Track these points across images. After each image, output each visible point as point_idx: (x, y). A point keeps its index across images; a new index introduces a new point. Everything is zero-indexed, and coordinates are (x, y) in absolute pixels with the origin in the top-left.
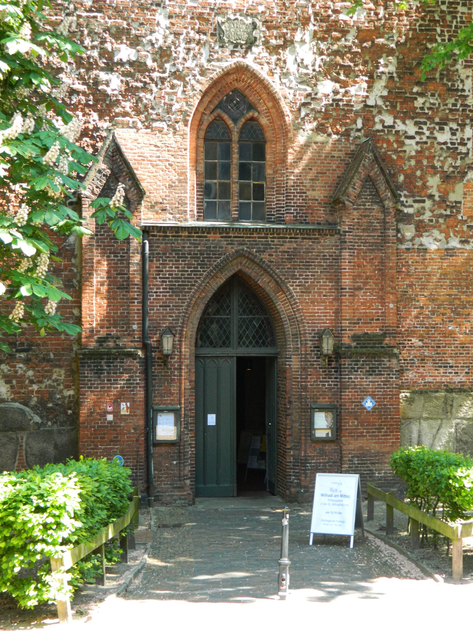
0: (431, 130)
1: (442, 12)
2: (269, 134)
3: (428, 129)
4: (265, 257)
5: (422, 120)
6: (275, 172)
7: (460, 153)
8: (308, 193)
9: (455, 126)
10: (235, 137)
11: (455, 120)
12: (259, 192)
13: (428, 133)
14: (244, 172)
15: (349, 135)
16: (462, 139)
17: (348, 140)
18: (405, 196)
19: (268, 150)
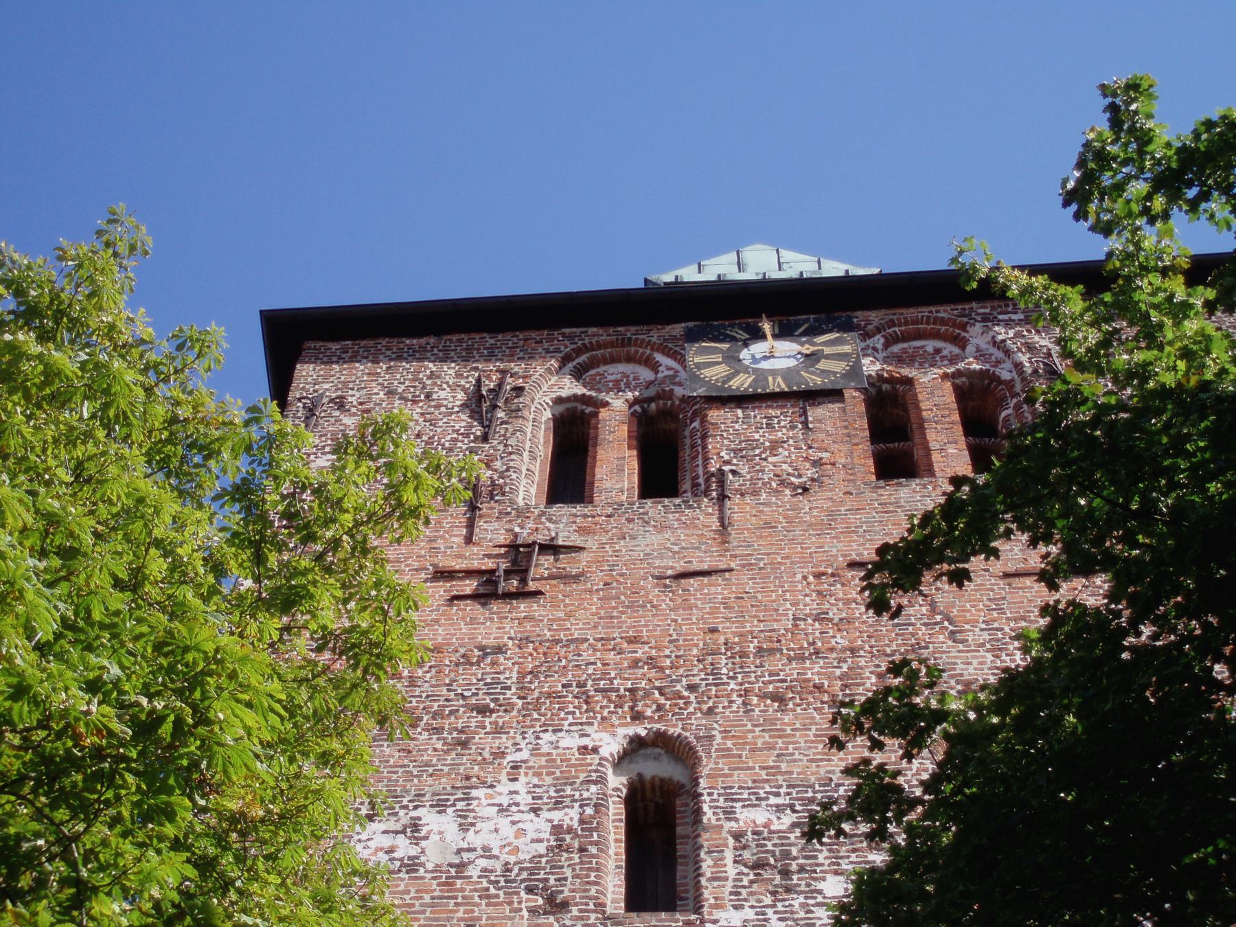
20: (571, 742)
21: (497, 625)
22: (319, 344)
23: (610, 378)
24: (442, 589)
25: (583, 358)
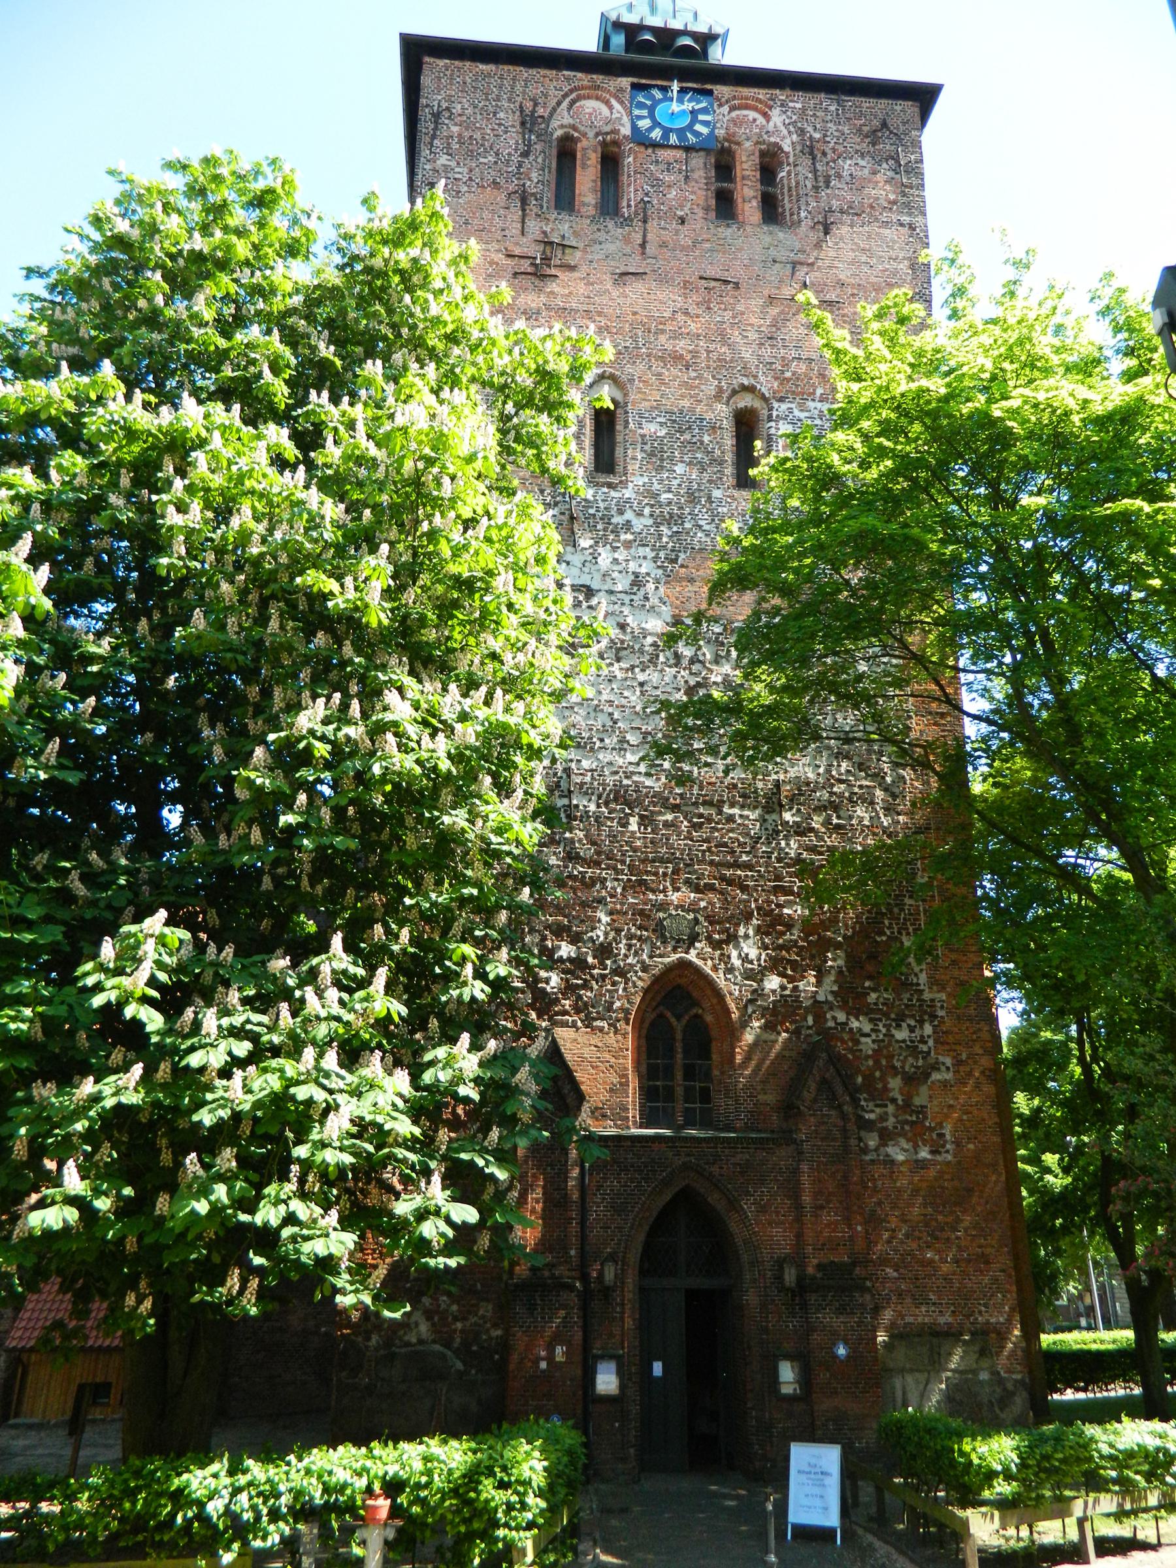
6: (722, 1073)
9: (913, 1023)
11: (913, 1016)
12: (705, 1095)
13: (884, 1030)
16: (922, 1036)
25: (573, 96)
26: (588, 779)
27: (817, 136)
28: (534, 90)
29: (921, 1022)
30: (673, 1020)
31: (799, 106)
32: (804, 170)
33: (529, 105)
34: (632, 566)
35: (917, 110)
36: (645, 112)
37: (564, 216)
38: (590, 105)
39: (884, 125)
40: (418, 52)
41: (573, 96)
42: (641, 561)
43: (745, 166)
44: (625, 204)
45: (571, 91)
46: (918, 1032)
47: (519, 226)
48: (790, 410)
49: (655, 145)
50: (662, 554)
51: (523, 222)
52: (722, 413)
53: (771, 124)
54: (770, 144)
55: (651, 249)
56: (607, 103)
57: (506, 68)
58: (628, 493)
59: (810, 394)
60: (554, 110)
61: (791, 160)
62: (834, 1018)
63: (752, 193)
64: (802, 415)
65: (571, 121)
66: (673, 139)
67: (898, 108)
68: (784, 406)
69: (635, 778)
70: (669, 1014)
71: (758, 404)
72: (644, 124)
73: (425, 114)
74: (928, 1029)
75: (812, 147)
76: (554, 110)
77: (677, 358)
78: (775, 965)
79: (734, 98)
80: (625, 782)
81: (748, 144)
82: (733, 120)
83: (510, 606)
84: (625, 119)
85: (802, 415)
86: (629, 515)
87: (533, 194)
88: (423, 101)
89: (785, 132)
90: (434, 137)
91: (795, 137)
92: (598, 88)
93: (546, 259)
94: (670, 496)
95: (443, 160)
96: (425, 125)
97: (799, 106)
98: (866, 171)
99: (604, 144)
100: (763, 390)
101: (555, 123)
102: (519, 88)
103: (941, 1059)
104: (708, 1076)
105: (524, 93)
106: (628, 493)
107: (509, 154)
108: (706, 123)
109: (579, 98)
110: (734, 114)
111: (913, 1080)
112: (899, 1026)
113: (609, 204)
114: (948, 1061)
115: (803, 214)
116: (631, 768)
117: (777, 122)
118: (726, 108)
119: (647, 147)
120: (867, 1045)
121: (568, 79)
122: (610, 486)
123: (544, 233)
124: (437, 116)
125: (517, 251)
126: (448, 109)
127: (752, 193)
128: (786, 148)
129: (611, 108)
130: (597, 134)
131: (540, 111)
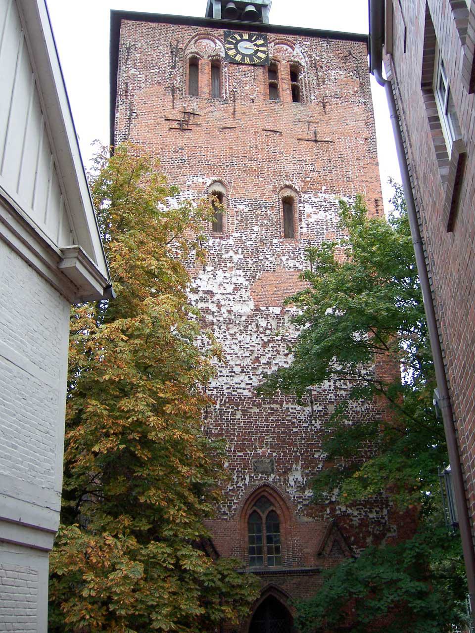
0: (366, 512)
1: (365, 451)
2: (282, 518)
3: (364, 511)
4: (284, 587)
5: (361, 507)
6: (286, 539)
7: (382, 523)
8: (304, 550)
9: (378, 509)
10: (264, 521)
11: (378, 506)
12: (278, 550)
13: (364, 514)
14: (270, 539)
15: (323, 517)
16: (382, 516)
17: (322, 519)
18: (356, 549)
19: (281, 527)
20: (201, 180)
21: (181, 140)
22: (126, 21)
23: (203, 44)
24: (167, 125)
25: (197, 38)
26: (215, 392)
27: (318, 58)
28: (176, 36)
29: (382, 509)
30: (261, 513)
31: (308, 43)
32: (312, 76)
33: (174, 43)
34: (234, 280)
35: (365, 46)
36: (232, 46)
37: (194, 99)
38: (205, 42)
39: (350, 53)
40: (118, 19)
41: (197, 38)
42: (238, 278)
43: (283, 73)
44: (224, 91)
45: (196, 36)
46: (380, 514)
47: (171, 104)
48: (310, 198)
49: (238, 64)
50: (248, 273)
51: (173, 102)
52: (276, 200)
53: (295, 52)
54: (294, 62)
55: (237, 115)
56: (213, 41)
57: (163, 25)
58: (231, 242)
59: (319, 189)
60: (187, 45)
61: (306, 70)
62: (340, 509)
63: (287, 86)
64: (316, 200)
65: (196, 50)
66: (247, 60)
67: (356, 45)
68: (307, 196)
69: (239, 391)
70: (259, 511)
71: (293, 194)
72: (232, 53)
73: (123, 49)
74: (385, 512)
75: (315, 64)
76: (187, 45)
77: (252, 170)
78: (308, 485)
79: (276, 39)
80: (234, 393)
81: (284, 62)
82: (276, 49)
83: (180, 167)
84: (223, 49)
85: (316, 200)
86: (231, 253)
87: (178, 88)
88: (121, 42)
89: (302, 56)
90: (127, 59)
91: (307, 59)
92: (209, 34)
93: (186, 122)
94: (251, 242)
95: (132, 71)
96: (123, 54)
97: (308, 43)
98: (342, 76)
99: (212, 61)
100: (296, 187)
101: (187, 52)
102: (169, 35)
103: (392, 526)
104: (278, 541)
105: (172, 37)
106: (231, 242)
107: (165, 68)
108: (264, 52)
109: (199, 39)
110: (276, 46)
111: (378, 539)
112: (371, 512)
113: (216, 93)
114: (395, 527)
115: (312, 98)
116: (236, 386)
117: (299, 52)
118: (273, 44)
119: (234, 64)
120: (356, 522)
121: (194, 30)
122: (221, 238)
123: (184, 107)
124: (128, 49)
125: (171, 117)
126: (134, 45)
127: (287, 86)
128: (303, 64)
129: (215, 43)
130: (209, 57)
131: (180, 46)
